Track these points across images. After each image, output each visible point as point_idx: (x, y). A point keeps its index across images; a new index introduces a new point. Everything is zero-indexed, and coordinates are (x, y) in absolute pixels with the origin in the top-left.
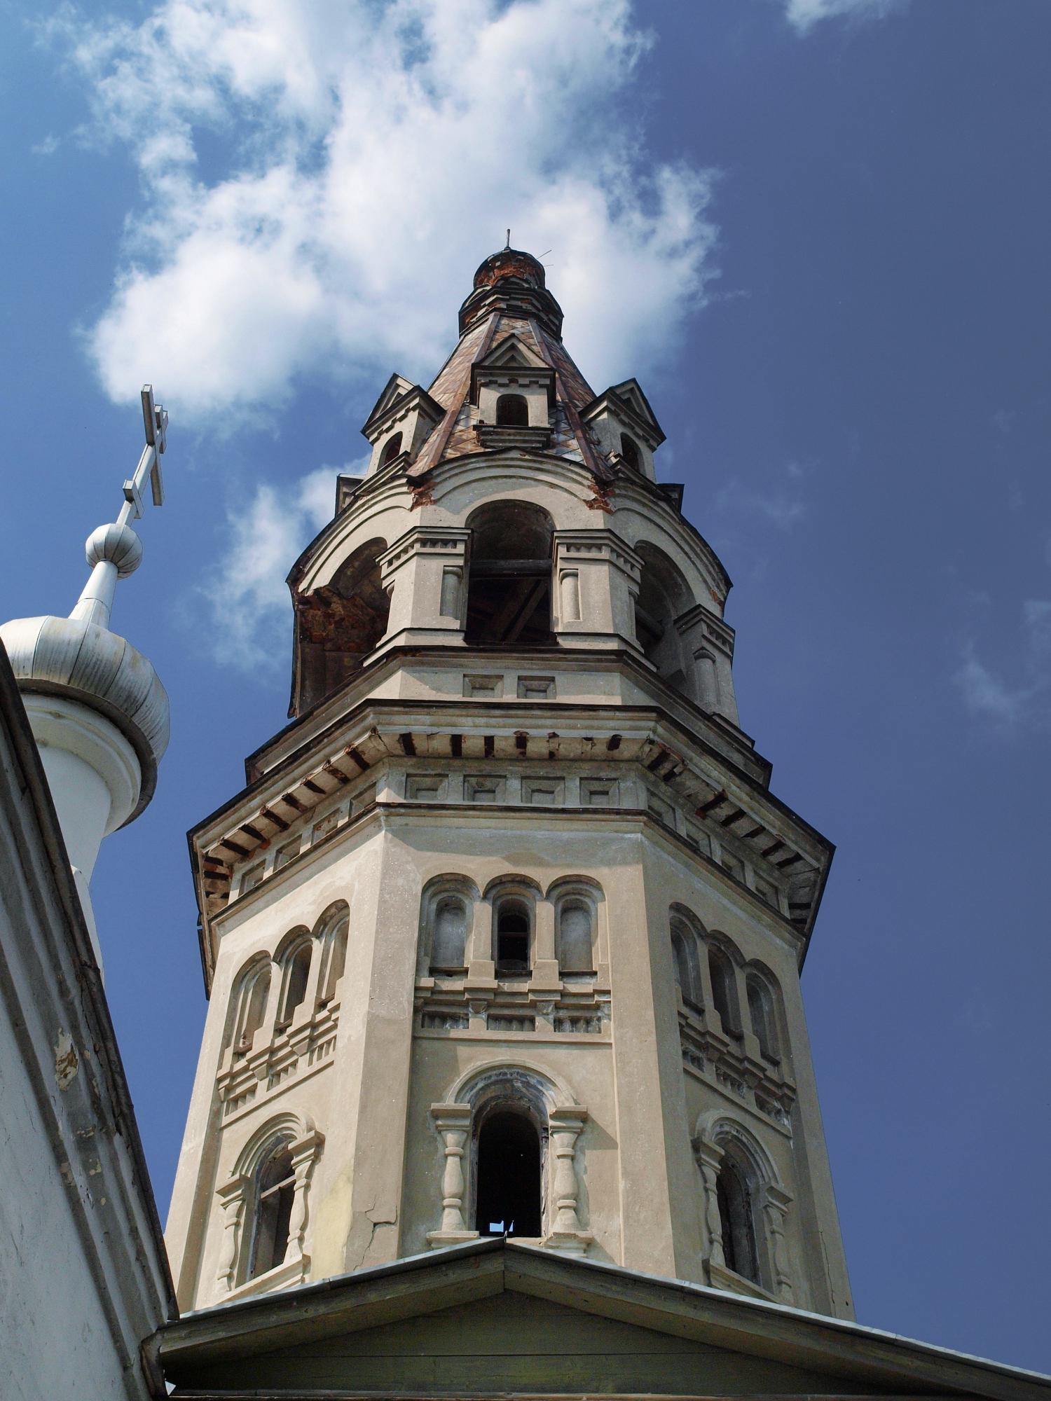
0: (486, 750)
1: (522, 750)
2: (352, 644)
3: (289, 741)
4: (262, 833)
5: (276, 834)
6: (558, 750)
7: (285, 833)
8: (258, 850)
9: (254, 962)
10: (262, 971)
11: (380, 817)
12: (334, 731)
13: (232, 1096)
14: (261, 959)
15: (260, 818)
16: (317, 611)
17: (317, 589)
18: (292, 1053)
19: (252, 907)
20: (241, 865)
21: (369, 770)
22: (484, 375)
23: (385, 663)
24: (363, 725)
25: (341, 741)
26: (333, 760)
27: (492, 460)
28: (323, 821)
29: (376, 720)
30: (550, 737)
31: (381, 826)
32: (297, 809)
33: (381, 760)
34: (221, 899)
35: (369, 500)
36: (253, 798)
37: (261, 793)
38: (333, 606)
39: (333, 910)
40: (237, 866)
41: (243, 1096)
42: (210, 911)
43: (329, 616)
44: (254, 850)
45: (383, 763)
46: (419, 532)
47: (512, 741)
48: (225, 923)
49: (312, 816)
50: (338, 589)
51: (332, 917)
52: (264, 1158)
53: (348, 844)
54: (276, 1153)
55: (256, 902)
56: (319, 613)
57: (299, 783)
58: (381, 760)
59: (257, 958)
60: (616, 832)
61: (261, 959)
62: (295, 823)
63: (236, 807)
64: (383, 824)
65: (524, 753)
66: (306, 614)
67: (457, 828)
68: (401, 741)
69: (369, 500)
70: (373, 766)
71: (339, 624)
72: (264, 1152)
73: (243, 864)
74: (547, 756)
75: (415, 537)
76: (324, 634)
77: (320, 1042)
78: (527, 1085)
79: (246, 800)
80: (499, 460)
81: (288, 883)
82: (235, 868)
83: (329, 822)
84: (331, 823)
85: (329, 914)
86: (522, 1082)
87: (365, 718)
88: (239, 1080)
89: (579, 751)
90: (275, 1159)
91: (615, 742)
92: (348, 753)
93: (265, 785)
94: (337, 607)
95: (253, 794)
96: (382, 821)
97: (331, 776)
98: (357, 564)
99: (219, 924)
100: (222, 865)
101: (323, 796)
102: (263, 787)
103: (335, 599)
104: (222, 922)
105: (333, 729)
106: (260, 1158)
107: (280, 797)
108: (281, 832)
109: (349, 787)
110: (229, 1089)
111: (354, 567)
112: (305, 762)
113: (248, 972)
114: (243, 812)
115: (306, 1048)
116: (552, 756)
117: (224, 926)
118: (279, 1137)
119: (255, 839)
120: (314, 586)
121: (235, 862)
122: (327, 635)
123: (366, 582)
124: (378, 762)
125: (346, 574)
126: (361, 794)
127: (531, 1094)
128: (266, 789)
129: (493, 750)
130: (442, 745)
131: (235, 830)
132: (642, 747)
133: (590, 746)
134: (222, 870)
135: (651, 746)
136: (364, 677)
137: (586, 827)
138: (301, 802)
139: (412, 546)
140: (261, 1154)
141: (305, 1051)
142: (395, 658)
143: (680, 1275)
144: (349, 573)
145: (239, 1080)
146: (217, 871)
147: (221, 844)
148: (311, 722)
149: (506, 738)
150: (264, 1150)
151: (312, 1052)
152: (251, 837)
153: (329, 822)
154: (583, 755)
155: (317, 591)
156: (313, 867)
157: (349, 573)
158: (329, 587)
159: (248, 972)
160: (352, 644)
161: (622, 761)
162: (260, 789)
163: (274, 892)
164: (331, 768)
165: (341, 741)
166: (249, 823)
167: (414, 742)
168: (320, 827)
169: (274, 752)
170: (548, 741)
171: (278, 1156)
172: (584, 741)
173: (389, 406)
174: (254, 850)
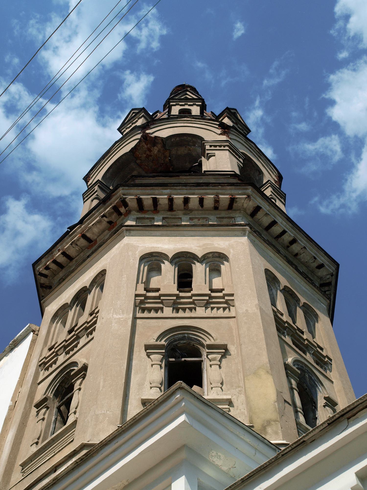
0: (278, 235)
1: (289, 245)
2: (147, 168)
3: (160, 180)
4: (159, 206)
5: (164, 210)
6: (300, 254)
7: (169, 213)
8: (150, 212)
9: (150, 255)
11: (246, 231)
12: (225, 186)
13: (142, 306)
15: (166, 199)
17: (157, 136)
18: (193, 303)
20: (136, 213)
21: (231, 211)
22: (228, 114)
23: (229, 177)
24: (245, 191)
25: (229, 192)
26: (221, 196)
27: (247, 141)
28: (196, 218)
29: (252, 193)
31: (245, 234)
32: (184, 206)
33: (240, 210)
34: (106, 223)
35: (192, 121)
36: (167, 189)
38: (155, 148)
39: (211, 255)
40: (133, 212)
43: (149, 150)
44: (148, 211)
45: (240, 212)
48: (131, 231)
50: (166, 142)
51: (208, 258)
52: (172, 342)
53: (222, 233)
54: (178, 343)
55: (156, 231)
57: (197, 196)
58: (240, 210)
59: (154, 254)
60: (318, 299)
62: (178, 211)
64: (247, 234)
65: (288, 247)
66: (141, 143)
68: (254, 208)
69: (192, 121)
70: (234, 210)
71: (148, 156)
73: (137, 213)
74: (294, 254)
75: (228, 144)
76: (140, 156)
77: (212, 306)
78: (310, 378)
79: (161, 188)
82: (132, 212)
83: (198, 220)
84: (200, 221)
85: (208, 255)
86: (309, 376)
87: (247, 189)
88: (148, 301)
89: (307, 260)
90: (177, 345)
91: (321, 266)
92: (231, 198)
93: (175, 187)
97: (213, 202)
98: (178, 139)
99: (127, 230)
100: (125, 208)
101: (201, 208)
103: (159, 146)
104: (130, 230)
105: (226, 185)
106: (170, 342)
107: (183, 196)
108: (168, 211)
109: (217, 212)
110: (142, 302)
111: (176, 139)
114: (157, 192)
117: (130, 233)
118: (185, 336)
119: (153, 206)
121: (134, 210)
122: (141, 157)
123: (176, 148)
124: (238, 210)
125: (172, 139)
126: (223, 218)
127: (310, 383)
128: (175, 189)
131: (149, 197)
132: (327, 275)
134: (122, 210)
135: (331, 276)
136: (215, 177)
137: (310, 290)
138: (189, 204)
139: (224, 146)
142: (234, 179)
145: (148, 301)
146: (120, 209)
148: (176, 179)
149: (290, 236)
150: (173, 339)
151: (206, 308)
152: (152, 204)
153: (198, 220)
154: (306, 263)
155: (156, 137)
156: (198, 233)
157: (172, 140)
158: (164, 139)
159: (146, 258)
160: (147, 168)
161: (316, 276)
163: (169, 232)
164: (218, 199)
166: (158, 198)
167: (259, 212)
168: (193, 220)
169: (148, 180)
170: (302, 248)
172: (313, 258)
173: (182, 98)
174: (148, 211)
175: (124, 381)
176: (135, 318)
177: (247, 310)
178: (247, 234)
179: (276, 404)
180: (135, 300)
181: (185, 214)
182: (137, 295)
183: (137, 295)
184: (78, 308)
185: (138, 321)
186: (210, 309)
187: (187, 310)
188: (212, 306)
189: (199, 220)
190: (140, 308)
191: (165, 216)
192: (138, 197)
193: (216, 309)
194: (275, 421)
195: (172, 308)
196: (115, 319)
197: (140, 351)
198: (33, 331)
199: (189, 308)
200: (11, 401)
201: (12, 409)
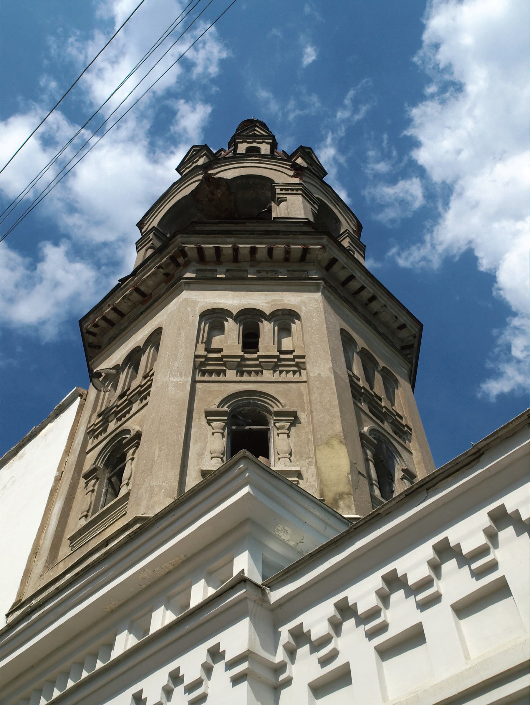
4: (222, 257)
10: (216, 319)
14: (217, 313)
16: (208, 188)
19: (214, 286)
30: (384, 305)
32: (251, 257)
37: (237, 237)
38: (219, 191)
39: (280, 312)
41: (211, 373)
42: (150, 277)
43: (212, 193)
46: (302, 187)
47: (370, 295)
48: (191, 285)
49: (257, 265)
56: (208, 189)
60: (399, 363)
61: (217, 313)
63: (216, 235)
64: (321, 290)
65: (367, 304)
67: (346, 315)
72: (237, 406)
73: (197, 265)
76: (201, 200)
78: (388, 449)
80: (324, 187)
81: (245, 286)
86: (386, 446)
87: (322, 238)
91: (403, 327)
93: (241, 236)
94: (219, 193)
95: (230, 235)
96: (321, 288)
98: (244, 181)
99: (185, 283)
100: (184, 258)
101: (269, 259)
102: (240, 236)
105: (298, 233)
107: (249, 246)
110: (202, 364)
112: (273, 238)
113: (207, 315)
114: (220, 240)
115: (272, 367)
116: (376, 313)
118: (250, 402)
120: (219, 175)
128: (241, 238)
129: (358, 294)
130: (343, 275)
132: (409, 336)
133: (394, 321)
134: (181, 260)
140: (235, 406)
141: (270, 369)
143: (216, 590)
144: (238, 182)
147: (197, 247)
150: (237, 405)
152: (215, 254)
155: (219, 178)
157: (238, 182)
159: (207, 315)
162: (238, 236)
165: (306, 242)
167: (335, 265)
170: (382, 307)
171: (243, 412)
175: (181, 450)
176: (194, 382)
177: (319, 374)
178: (321, 290)
179: (350, 476)
180: (195, 361)
181: (252, 266)
182: (196, 357)
183: (196, 357)
184: (130, 370)
185: (198, 385)
186: (278, 372)
187: (253, 373)
188: (280, 369)
189: (267, 273)
190: (200, 371)
191: (229, 268)
192: (199, 246)
193: (285, 372)
194: (348, 494)
195: (235, 371)
196: (172, 382)
197: (199, 418)
198: (81, 396)
199: (255, 371)
200: (58, 470)
201: (58, 479)
